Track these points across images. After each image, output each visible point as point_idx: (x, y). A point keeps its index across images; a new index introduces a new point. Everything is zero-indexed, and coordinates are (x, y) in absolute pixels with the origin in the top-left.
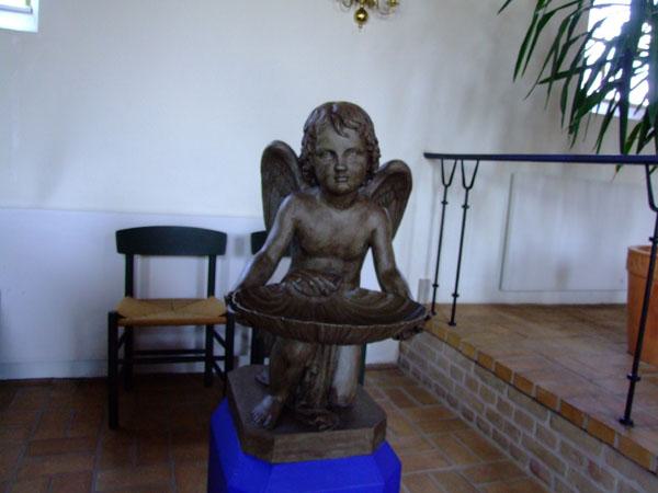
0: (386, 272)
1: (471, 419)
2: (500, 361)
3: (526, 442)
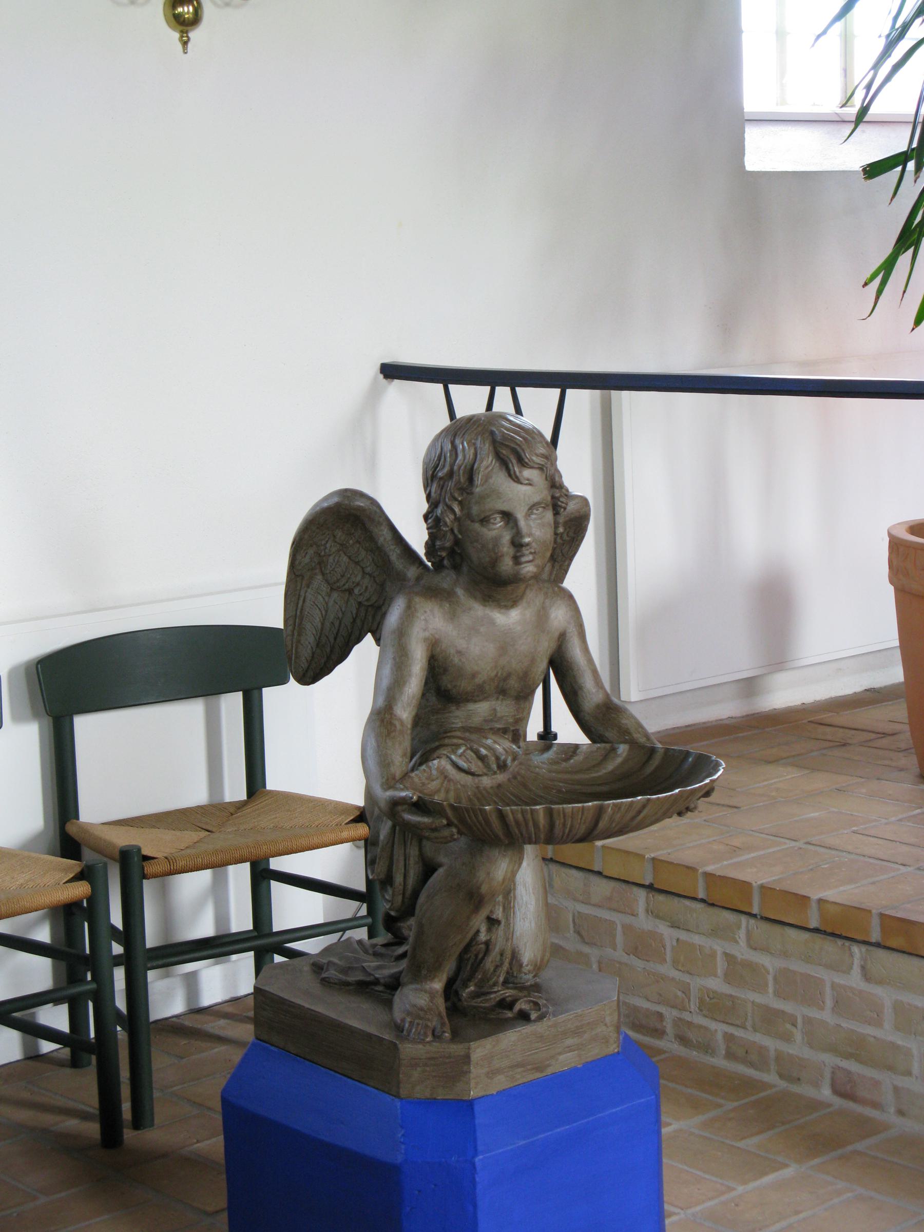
0: (598, 706)
1: (659, 1033)
2: (710, 868)
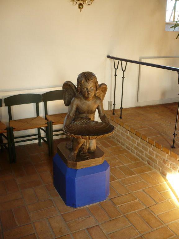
0: (103, 116)
1: (129, 149)
3: (146, 154)
